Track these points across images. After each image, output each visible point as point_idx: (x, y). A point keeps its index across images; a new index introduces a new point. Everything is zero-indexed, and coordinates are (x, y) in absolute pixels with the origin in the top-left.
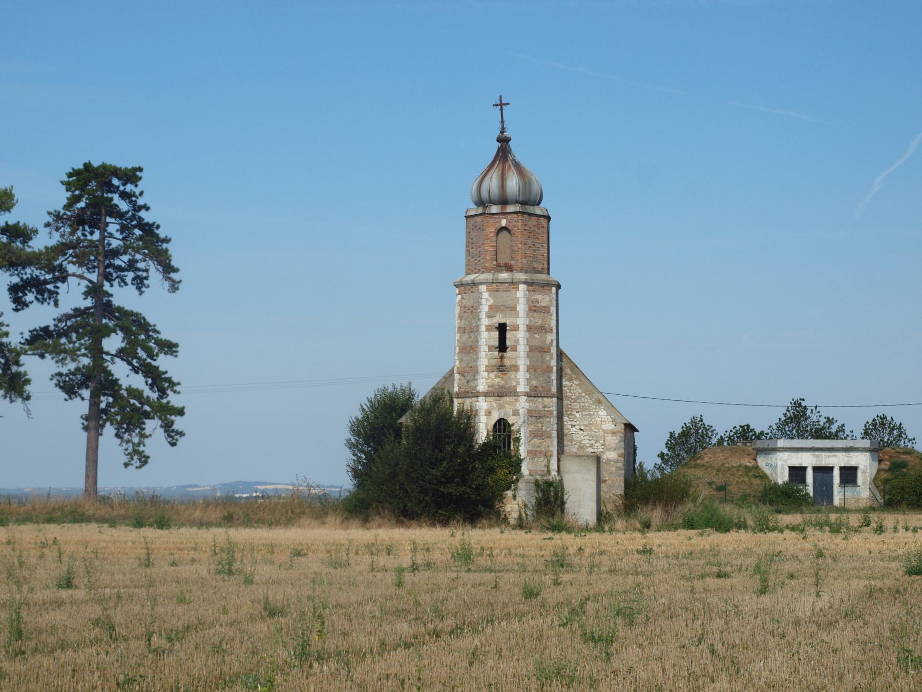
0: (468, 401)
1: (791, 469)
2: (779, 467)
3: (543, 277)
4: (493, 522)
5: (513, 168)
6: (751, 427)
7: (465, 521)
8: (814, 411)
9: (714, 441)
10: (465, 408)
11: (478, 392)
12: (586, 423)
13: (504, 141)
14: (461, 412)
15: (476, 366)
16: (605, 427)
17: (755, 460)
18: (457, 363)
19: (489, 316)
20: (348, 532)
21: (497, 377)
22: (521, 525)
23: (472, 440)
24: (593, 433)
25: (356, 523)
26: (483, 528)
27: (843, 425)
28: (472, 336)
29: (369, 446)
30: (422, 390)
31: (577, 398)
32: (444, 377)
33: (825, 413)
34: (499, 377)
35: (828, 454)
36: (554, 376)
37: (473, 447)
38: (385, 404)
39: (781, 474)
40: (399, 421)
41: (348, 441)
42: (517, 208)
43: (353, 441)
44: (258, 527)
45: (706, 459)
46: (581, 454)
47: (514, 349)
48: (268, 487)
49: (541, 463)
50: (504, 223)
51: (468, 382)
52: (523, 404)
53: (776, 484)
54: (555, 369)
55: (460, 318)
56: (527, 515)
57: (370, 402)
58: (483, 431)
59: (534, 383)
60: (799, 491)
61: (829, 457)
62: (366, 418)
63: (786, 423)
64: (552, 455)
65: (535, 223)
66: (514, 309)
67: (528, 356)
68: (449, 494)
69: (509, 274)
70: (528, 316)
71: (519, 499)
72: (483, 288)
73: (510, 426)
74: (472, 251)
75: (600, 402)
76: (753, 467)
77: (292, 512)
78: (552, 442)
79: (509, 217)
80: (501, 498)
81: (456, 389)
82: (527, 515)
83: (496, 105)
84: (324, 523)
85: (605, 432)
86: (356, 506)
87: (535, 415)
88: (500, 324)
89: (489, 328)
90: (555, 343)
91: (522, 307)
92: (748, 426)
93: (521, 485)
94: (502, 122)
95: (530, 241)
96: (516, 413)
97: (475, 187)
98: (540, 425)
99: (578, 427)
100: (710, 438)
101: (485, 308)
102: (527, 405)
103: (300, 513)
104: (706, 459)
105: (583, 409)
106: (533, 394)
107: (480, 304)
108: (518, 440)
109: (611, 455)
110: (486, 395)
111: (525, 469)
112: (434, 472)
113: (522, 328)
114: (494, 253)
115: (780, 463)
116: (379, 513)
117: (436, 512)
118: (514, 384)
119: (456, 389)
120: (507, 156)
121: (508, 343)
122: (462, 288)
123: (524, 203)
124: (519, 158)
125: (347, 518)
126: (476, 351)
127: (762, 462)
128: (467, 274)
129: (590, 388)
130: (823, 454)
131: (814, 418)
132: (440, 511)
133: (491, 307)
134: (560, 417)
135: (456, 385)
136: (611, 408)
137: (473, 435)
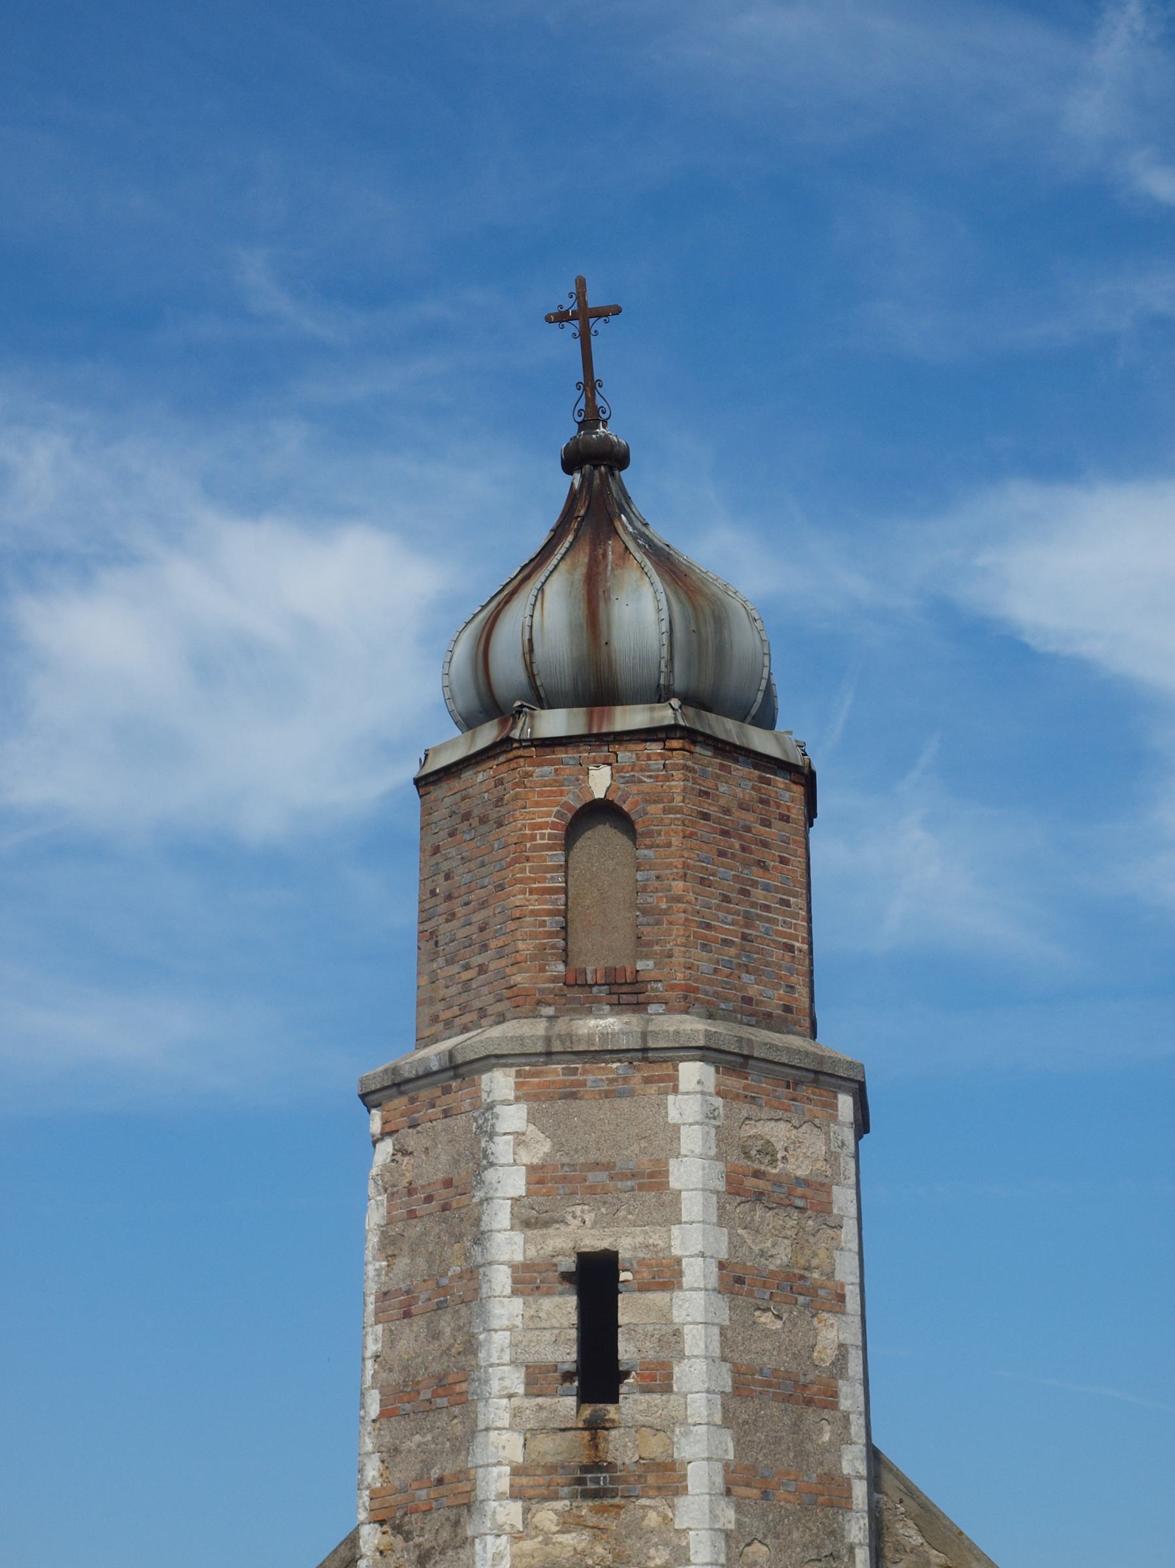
5: (639, 555)
15: (465, 1475)
19: (530, 1220)
21: (568, 1523)
28: (446, 1323)
34: (580, 1524)
47: (659, 1380)
50: (600, 782)
55: (390, 1245)
65: (746, 792)
66: (653, 1180)
67: (728, 1420)
70: (723, 1218)
72: (500, 1083)
79: (625, 755)
83: (561, 317)
89: (528, 1280)
90: (854, 1366)
91: (692, 1173)
94: (590, 385)
95: (725, 874)
97: (463, 650)
101: (509, 1182)
107: (483, 1161)
113: (696, 1273)
114: (552, 924)
121: (626, 1351)
122: (400, 1103)
123: (690, 700)
124: (660, 533)
128: (423, 1041)
133: (537, 1175)
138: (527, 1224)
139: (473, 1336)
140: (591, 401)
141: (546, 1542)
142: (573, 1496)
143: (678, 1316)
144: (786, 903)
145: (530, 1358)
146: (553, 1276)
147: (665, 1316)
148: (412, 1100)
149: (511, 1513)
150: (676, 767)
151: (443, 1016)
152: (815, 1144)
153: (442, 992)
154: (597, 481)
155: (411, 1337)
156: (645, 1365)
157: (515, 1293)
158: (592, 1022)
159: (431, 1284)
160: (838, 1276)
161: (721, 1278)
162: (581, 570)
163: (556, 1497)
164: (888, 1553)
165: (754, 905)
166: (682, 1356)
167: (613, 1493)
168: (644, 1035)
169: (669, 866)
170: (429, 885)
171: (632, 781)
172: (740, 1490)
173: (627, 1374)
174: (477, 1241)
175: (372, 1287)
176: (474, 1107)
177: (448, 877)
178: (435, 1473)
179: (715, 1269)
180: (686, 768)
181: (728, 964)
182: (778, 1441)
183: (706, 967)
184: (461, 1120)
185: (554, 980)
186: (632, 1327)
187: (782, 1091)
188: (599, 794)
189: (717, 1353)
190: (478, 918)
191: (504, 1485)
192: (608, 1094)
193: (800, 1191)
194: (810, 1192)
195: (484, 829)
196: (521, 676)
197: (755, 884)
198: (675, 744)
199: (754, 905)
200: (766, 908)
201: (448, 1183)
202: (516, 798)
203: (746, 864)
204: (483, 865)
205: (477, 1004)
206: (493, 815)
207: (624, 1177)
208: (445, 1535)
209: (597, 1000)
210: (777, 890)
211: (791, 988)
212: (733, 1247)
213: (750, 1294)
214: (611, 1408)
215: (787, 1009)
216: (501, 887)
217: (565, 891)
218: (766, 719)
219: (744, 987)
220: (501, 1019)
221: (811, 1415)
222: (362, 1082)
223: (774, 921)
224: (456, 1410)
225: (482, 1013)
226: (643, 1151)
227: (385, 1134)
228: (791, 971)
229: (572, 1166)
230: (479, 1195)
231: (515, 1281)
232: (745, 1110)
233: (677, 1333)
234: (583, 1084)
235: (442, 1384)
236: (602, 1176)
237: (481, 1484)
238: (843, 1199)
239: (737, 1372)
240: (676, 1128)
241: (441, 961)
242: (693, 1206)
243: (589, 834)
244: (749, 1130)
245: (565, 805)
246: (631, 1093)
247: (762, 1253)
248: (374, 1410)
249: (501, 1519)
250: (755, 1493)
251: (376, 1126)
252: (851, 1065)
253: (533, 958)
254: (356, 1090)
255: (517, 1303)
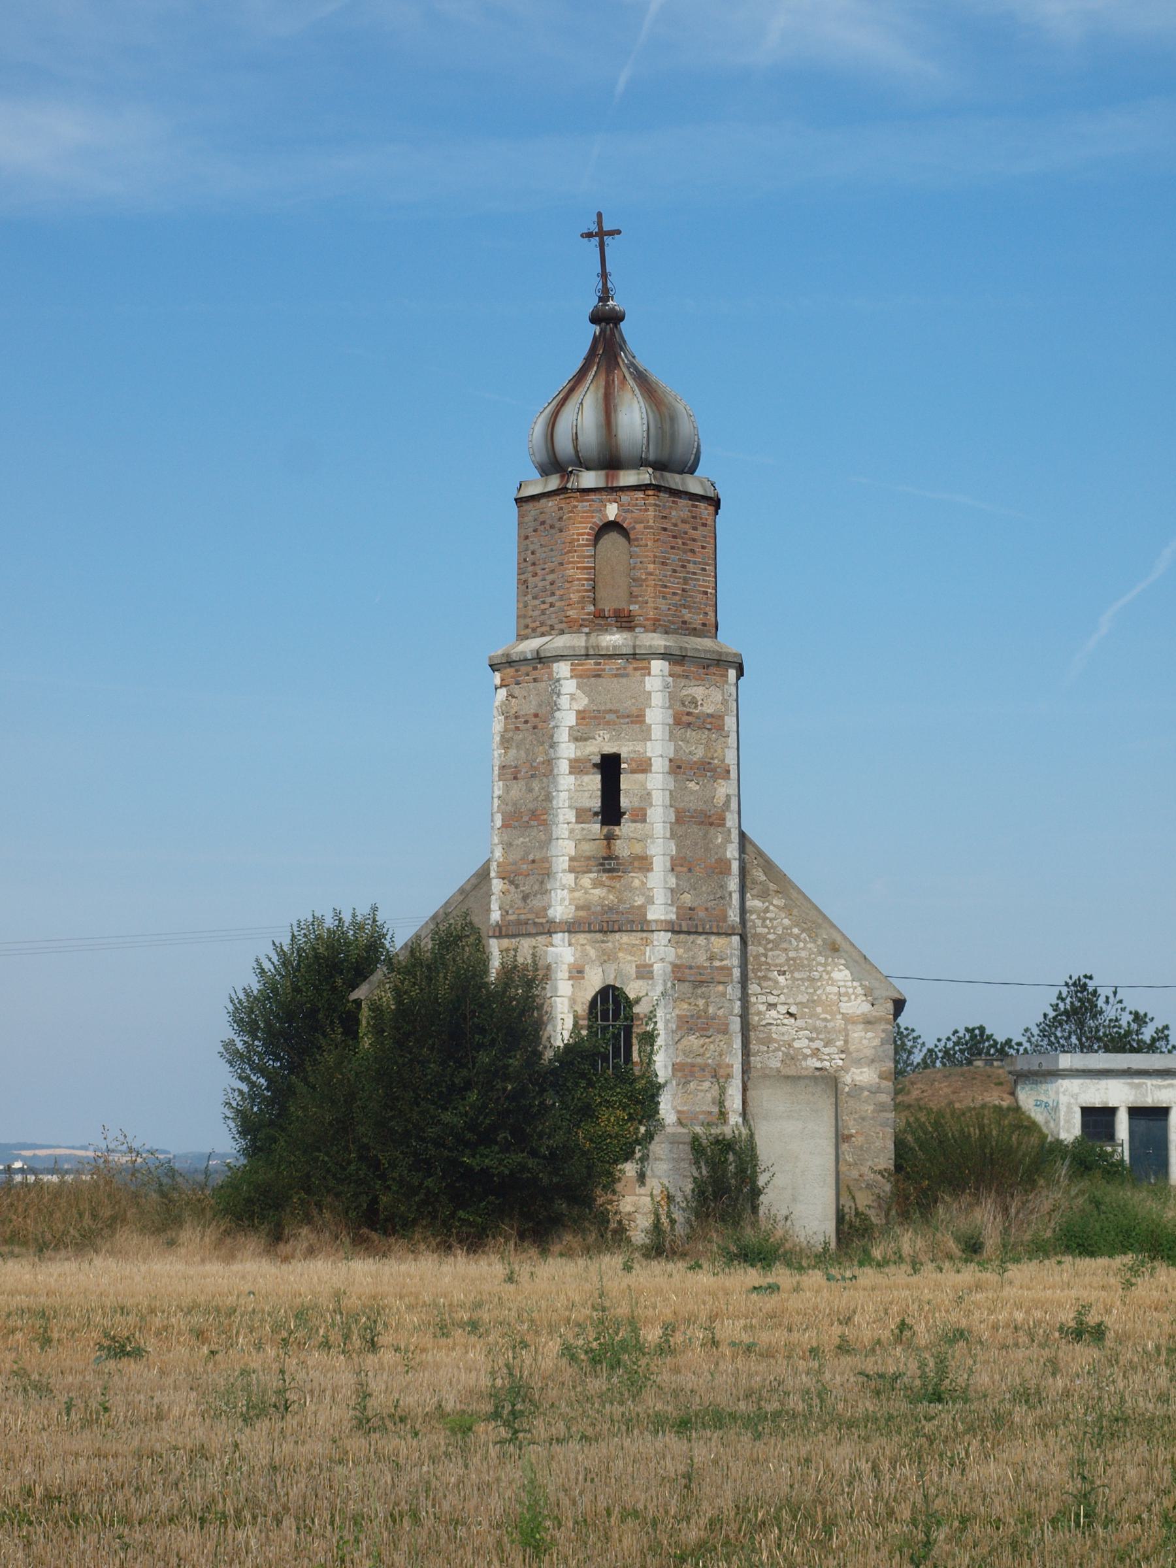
0: (526, 944)
1: (1087, 1111)
2: (1063, 1109)
3: (706, 643)
4: (592, 1238)
5: (631, 382)
6: (988, 1032)
7: (522, 1236)
8: (1111, 1000)
9: (917, 1058)
10: (520, 960)
11: (552, 922)
12: (804, 998)
13: (607, 319)
14: (510, 972)
15: (546, 860)
16: (847, 1007)
17: (1013, 1094)
18: (498, 853)
19: (578, 738)
20: (236, 1267)
21: (597, 884)
22: (659, 1247)
23: (537, 1038)
24: (819, 1024)
25: (253, 1243)
26: (567, 1254)
27: (1166, 1027)
28: (536, 785)
29: (277, 1058)
30: (404, 925)
31: (781, 938)
32: (462, 891)
33: (1135, 1001)
35: (1158, 1082)
36: (733, 884)
37: (540, 1055)
38: (317, 957)
39: (1067, 1121)
40: (354, 996)
41: (228, 1045)
42: (645, 476)
43: (240, 1045)
44: (12, 1255)
45: (915, 1093)
46: (791, 1071)
47: (640, 816)
48: (41, 1153)
49: (703, 1095)
50: (612, 511)
51: (525, 898)
52: (661, 951)
53: (1059, 1142)
54: (735, 866)
55: (506, 742)
56: (673, 1222)
57: (281, 953)
58: (564, 1016)
59: (687, 899)
60: (1104, 1156)
61: (1160, 1087)
62: (271, 989)
63: (1056, 1022)
64: (729, 1076)
65: (685, 514)
66: (638, 719)
67: (673, 835)
68: (485, 1171)
69: (626, 635)
71: (654, 1184)
72: (562, 669)
73: (630, 1004)
74: (532, 581)
75: (835, 949)
76: (1009, 1109)
77: (94, 1217)
78: (729, 1044)
79: (625, 498)
80: (611, 1182)
81: (496, 916)
82: (673, 1222)
83: (589, 235)
84: (172, 1243)
85: (848, 1019)
86: (249, 1201)
87: (689, 979)
88: (605, 757)
89: (577, 767)
90: (734, 805)
91: (657, 716)
92: (982, 1029)
93: (658, 1148)
94: (604, 275)
95: (674, 558)
96: (644, 972)
97: (539, 429)
98: (701, 1002)
99: (783, 1009)
100: (910, 1053)
101: (567, 718)
102: (671, 954)
103: (114, 1218)
104: (915, 1093)
105: (795, 965)
106: (685, 927)
107: (554, 708)
108: (649, 1038)
109: (865, 1075)
110: (572, 928)
111: (667, 1108)
112: (447, 1117)
113: (659, 765)
114: (587, 585)
115: (1063, 1100)
116: (308, 1220)
117: (453, 1215)
118: (639, 901)
119: (496, 916)
120: (616, 357)
121: (624, 802)
122: (510, 671)
123: (660, 466)
124: (642, 362)
125: (227, 1233)
126: (545, 823)
127: (1027, 1098)
128: (522, 638)
129: (813, 920)
130: (1149, 1082)
131: (1110, 1012)
132: (461, 1214)
133: (581, 715)
134: (744, 982)
135: (495, 906)
136: (862, 964)
137: (539, 1025)
138: (576, 739)
139: (550, 793)
140: (605, 284)
141: (586, 893)
142: (599, 872)
143: (650, 786)
144: (704, 570)
145: (578, 805)
146: (589, 765)
147: (643, 785)
148: (517, 671)
149: (569, 879)
150: (650, 505)
151: (531, 625)
152: (717, 696)
153: (531, 613)
154: (608, 332)
155: (517, 790)
156: (634, 809)
157: (571, 773)
158: (608, 638)
159: (528, 765)
160: (727, 762)
161: (670, 767)
162: (602, 391)
163: (591, 872)
164: (748, 883)
165: (688, 573)
166: (651, 805)
167: (617, 870)
168: (634, 647)
169: (647, 556)
170: (523, 556)
171: (628, 511)
172: (678, 869)
173: (624, 813)
174: (551, 747)
175: (497, 763)
176: (550, 679)
177: (533, 553)
178: (531, 857)
179: (667, 763)
180: (656, 505)
181: (675, 605)
182: (696, 844)
183: (664, 607)
184: (543, 685)
185: (589, 614)
186: (627, 791)
187: (701, 671)
188: (612, 518)
189: (668, 803)
190: (550, 577)
191: (566, 866)
192: (616, 676)
193: (709, 720)
194: (713, 720)
195: (553, 531)
196: (570, 450)
197: (689, 562)
198: (650, 492)
199: (688, 573)
200: (695, 574)
201: (536, 715)
202: (569, 518)
203: (685, 552)
204: (552, 550)
205: (549, 622)
206: (558, 525)
207: (624, 717)
208: (536, 887)
209: (610, 625)
210: (700, 563)
211: (706, 614)
212: (676, 751)
213: (684, 773)
214: (616, 828)
215: (704, 625)
216: (561, 564)
217: (594, 568)
218: (713, 629)
219: (682, 617)
220: (562, 632)
221: (712, 830)
222: (490, 658)
223: (698, 580)
224: (541, 828)
225: (552, 627)
226: (633, 704)
227: (502, 686)
228: (706, 605)
229: (599, 711)
230: (552, 724)
231: (571, 767)
232: (683, 682)
233: (649, 794)
234: (604, 670)
235: (534, 815)
236: (613, 717)
237: (554, 865)
238: (730, 722)
239: (677, 812)
240: (650, 693)
241: (530, 596)
242: (658, 732)
243: (606, 537)
244: (684, 692)
245: (594, 523)
246: (627, 675)
247: (690, 753)
248: (499, 823)
249: (564, 882)
250: (685, 869)
251: (498, 681)
252: (736, 655)
253: (579, 602)
254: (487, 662)
255: (571, 779)
